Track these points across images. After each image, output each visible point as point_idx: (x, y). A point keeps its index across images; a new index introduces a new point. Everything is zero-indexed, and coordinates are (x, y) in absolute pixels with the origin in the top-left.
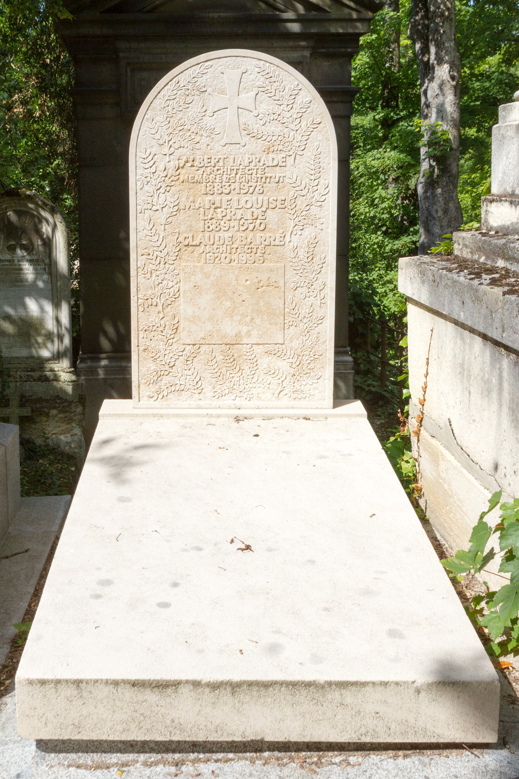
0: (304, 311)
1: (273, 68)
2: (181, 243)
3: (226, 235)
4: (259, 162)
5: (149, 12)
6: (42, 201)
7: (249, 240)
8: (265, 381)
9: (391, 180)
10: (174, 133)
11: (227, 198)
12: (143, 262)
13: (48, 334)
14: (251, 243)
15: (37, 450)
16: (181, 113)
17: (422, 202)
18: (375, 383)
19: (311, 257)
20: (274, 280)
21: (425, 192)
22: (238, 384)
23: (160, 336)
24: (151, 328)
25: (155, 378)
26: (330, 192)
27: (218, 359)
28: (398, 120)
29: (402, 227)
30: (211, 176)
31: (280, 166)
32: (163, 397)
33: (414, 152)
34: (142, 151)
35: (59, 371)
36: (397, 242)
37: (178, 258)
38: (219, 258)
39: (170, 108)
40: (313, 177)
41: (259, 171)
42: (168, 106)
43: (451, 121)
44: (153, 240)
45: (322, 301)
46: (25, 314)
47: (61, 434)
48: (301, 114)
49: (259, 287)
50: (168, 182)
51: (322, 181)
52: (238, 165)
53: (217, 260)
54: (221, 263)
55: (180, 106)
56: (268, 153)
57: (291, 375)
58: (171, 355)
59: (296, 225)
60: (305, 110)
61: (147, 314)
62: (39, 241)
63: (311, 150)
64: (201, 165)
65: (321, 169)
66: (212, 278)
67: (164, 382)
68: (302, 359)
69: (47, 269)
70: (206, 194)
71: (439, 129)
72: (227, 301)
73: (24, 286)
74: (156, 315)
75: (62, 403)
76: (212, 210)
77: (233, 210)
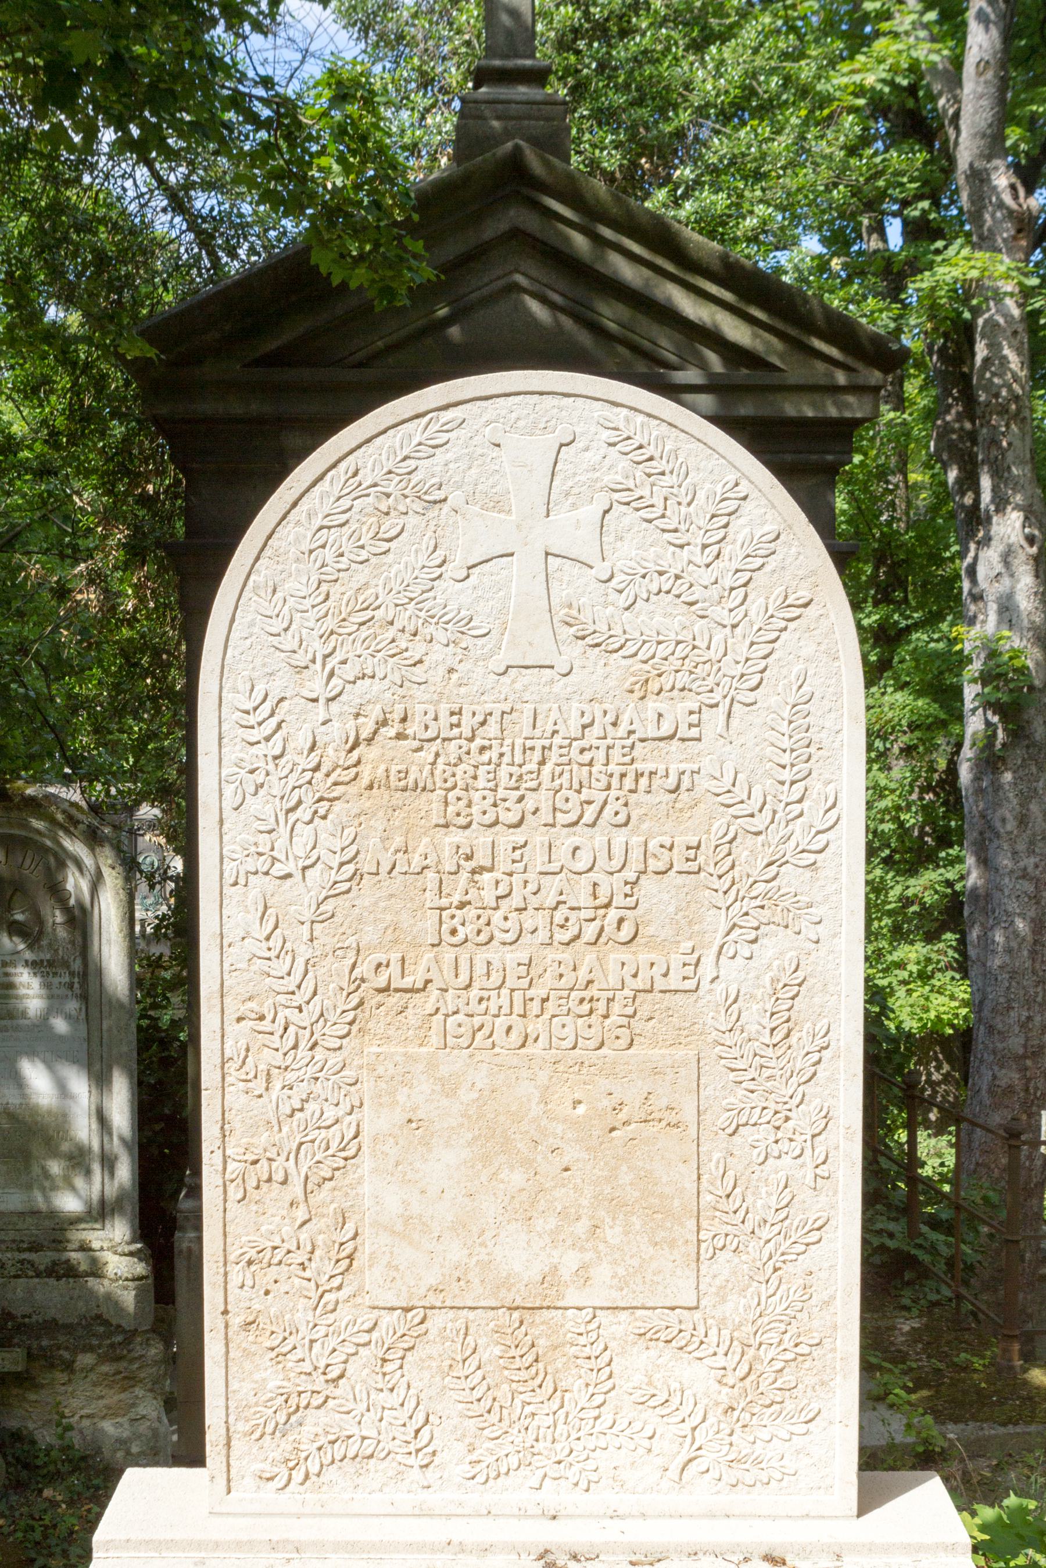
0: (763, 1202)
1: (659, 430)
2: (363, 980)
3: (509, 956)
4: (614, 724)
5: (360, 365)
6: (64, 812)
7: (583, 974)
8: (637, 1426)
9: (896, 750)
10: (341, 631)
11: (512, 838)
12: (242, 1044)
13: (76, 1153)
14: (590, 982)
15: (39, 1462)
16: (366, 569)
17: (971, 800)
18: (892, 1226)
19: (784, 1029)
20: (664, 1103)
21: (977, 779)
22: (549, 1438)
23: (297, 1281)
24: (268, 1253)
25: (281, 1418)
26: (843, 821)
27: (485, 1357)
28: (908, 629)
29: (921, 848)
30: (459, 770)
31: (683, 740)
32: (307, 1477)
33: (948, 696)
34: (241, 687)
35: (102, 1249)
36: (912, 882)
37: (355, 1028)
38: (486, 1031)
39: (329, 554)
40: (786, 775)
41: (616, 754)
42: (323, 546)
43: (1029, 629)
44: (273, 973)
45: (818, 1171)
46: (17, 1101)
47: (103, 1418)
48: (749, 574)
49: (617, 1124)
50: (322, 787)
51: (815, 785)
52: (548, 734)
53: (479, 1036)
54: (494, 1046)
55: (362, 547)
56: (643, 698)
57: (720, 1410)
58: (332, 1342)
59: (735, 925)
60: (759, 561)
61: (254, 1208)
62: (58, 913)
63: (780, 689)
64: (430, 734)
65: (812, 749)
66: (466, 1096)
67: (308, 1429)
68: (756, 1358)
69: (76, 986)
70: (446, 826)
71: (1005, 646)
72: (512, 1168)
73: (17, 1028)
74: (284, 1212)
75: (108, 1335)
76: (464, 875)
77: (531, 876)
